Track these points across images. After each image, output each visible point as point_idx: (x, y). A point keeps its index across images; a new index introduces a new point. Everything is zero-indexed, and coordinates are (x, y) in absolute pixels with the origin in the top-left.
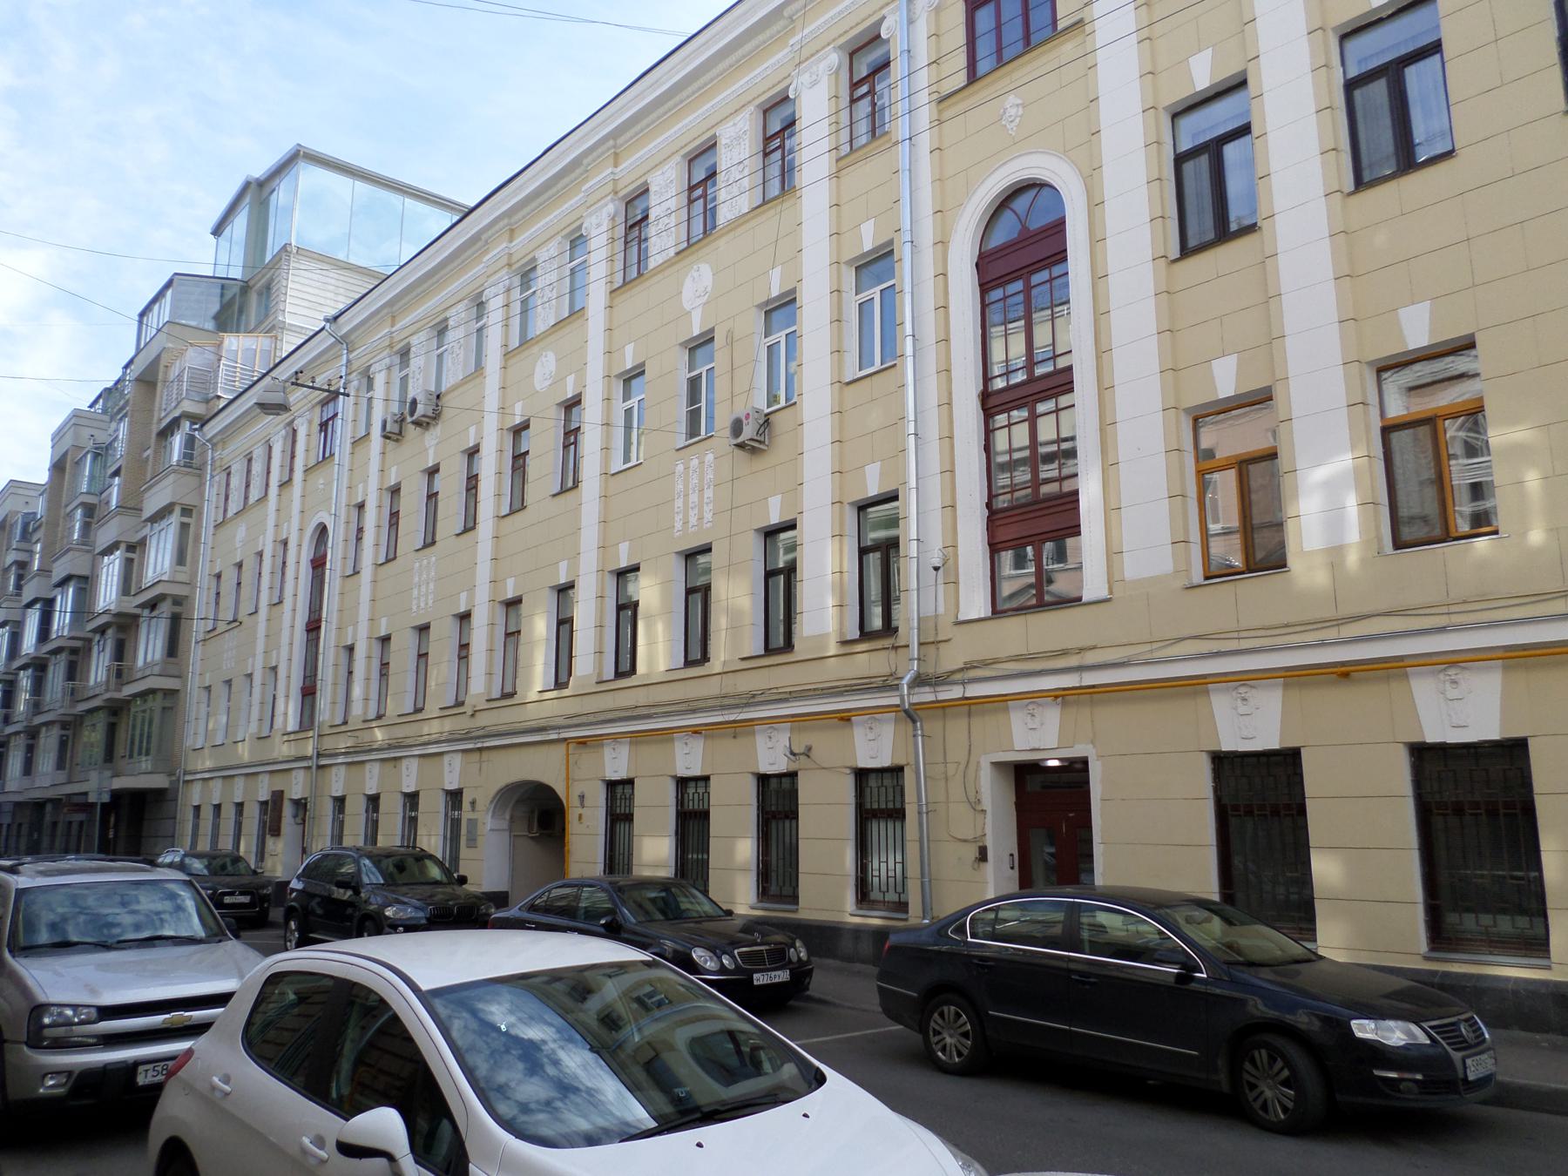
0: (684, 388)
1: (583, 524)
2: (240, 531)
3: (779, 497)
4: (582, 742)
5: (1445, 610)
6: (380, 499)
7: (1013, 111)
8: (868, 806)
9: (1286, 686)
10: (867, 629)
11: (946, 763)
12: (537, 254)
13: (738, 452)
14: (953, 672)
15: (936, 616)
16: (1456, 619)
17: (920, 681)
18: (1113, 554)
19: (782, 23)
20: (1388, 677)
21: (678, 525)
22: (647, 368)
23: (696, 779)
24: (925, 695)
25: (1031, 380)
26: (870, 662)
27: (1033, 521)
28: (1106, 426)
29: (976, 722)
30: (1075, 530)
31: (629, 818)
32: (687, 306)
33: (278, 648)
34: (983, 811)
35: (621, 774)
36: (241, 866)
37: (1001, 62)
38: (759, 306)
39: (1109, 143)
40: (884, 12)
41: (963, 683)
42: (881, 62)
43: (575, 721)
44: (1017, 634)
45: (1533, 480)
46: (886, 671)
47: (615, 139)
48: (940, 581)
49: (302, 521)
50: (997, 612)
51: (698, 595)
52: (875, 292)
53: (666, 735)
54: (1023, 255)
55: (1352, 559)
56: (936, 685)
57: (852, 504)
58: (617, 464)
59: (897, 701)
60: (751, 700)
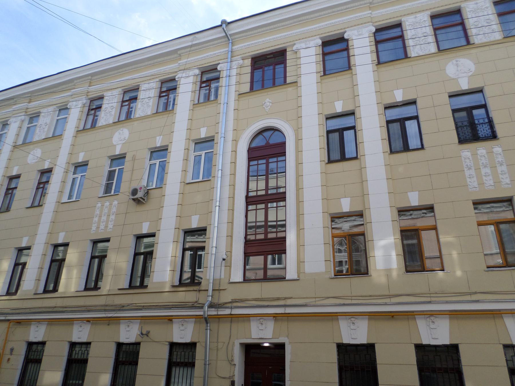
0: (106, 174)
1: (42, 222)
4: (19, 322)
5: (429, 295)
7: (268, 104)
8: (174, 360)
9: (369, 319)
10: (132, 285)
11: (218, 342)
13: (132, 201)
14: (226, 303)
15: (220, 279)
17: (211, 306)
18: (300, 262)
19: (176, 55)
20: (494, 318)
21: (94, 228)
22: (127, 156)
23: (81, 344)
24: (213, 312)
25: (267, 194)
26: (186, 296)
27: (266, 245)
28: (299, 215)
29: (234, 325)
30: (284, 252)
31: (39, 361)
34: (235, 365)
37: (263, 87)
38: (149, 149)
39: (305, 121)
40: (295, 42)
41: (231, 308)
42: (174, 87)
43: (17, 311)
44: (255, 290)
45: (455, 254)
46: (195, 300)
47: (92, 77)
48: (223, 265)
50: (246, 280)
51: (98, 259)
52: (157, 162)
53: (70, 322)
54: (268, 150)
55: (395, 274)
56: (218, 308)
57: (183, 230)
58: (65, 199)
59: (201, 313)
60: (122, 308)
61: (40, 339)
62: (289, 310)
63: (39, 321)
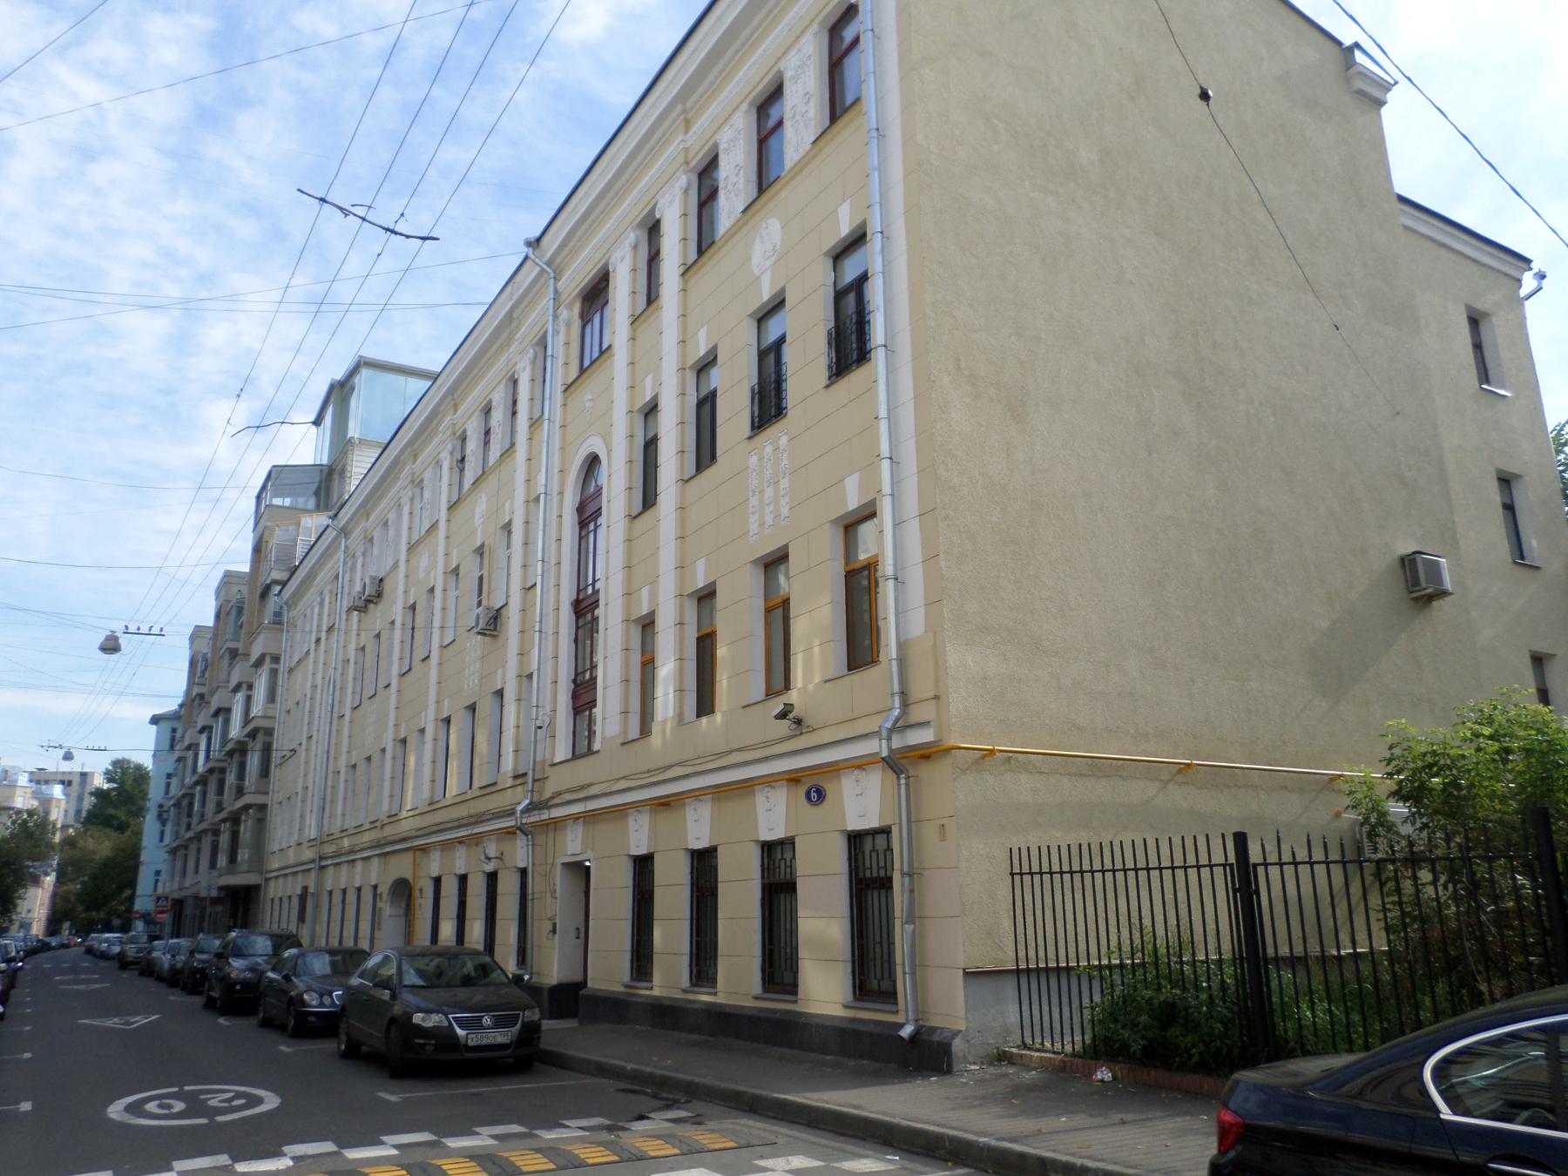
2: (481, 504)
3: (856, 476)
6: (632, 426)
12: (782, 66)
16: (699, 768)
21: (754, 528)
24: (534, 818)
32: (756, 272)
33: (653, 581)
35: (778, 834)
36: (495, 975)
47: (684, 103)
49: (563, 461)
60: (478, 819)
61: (872, 822)
62: (592, 805)
63: (859, 764)
